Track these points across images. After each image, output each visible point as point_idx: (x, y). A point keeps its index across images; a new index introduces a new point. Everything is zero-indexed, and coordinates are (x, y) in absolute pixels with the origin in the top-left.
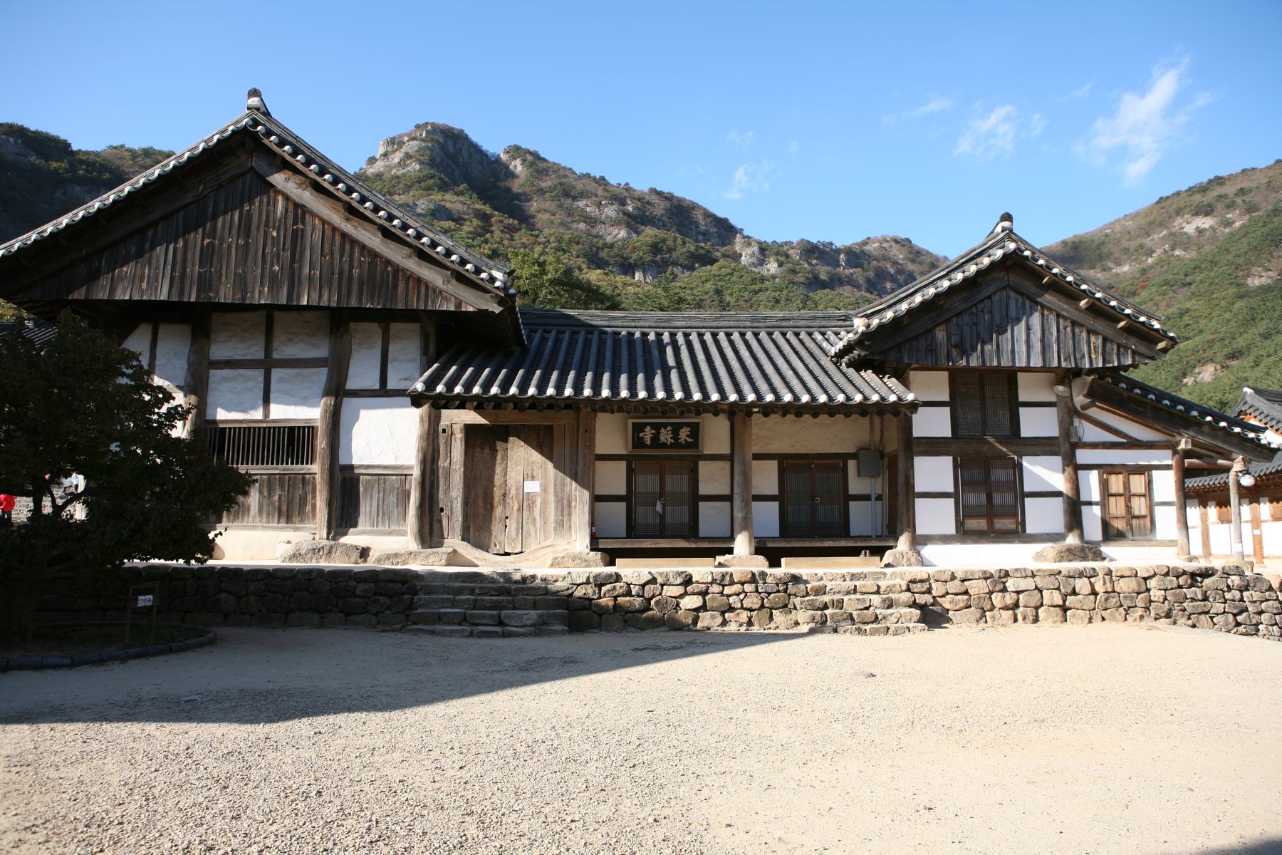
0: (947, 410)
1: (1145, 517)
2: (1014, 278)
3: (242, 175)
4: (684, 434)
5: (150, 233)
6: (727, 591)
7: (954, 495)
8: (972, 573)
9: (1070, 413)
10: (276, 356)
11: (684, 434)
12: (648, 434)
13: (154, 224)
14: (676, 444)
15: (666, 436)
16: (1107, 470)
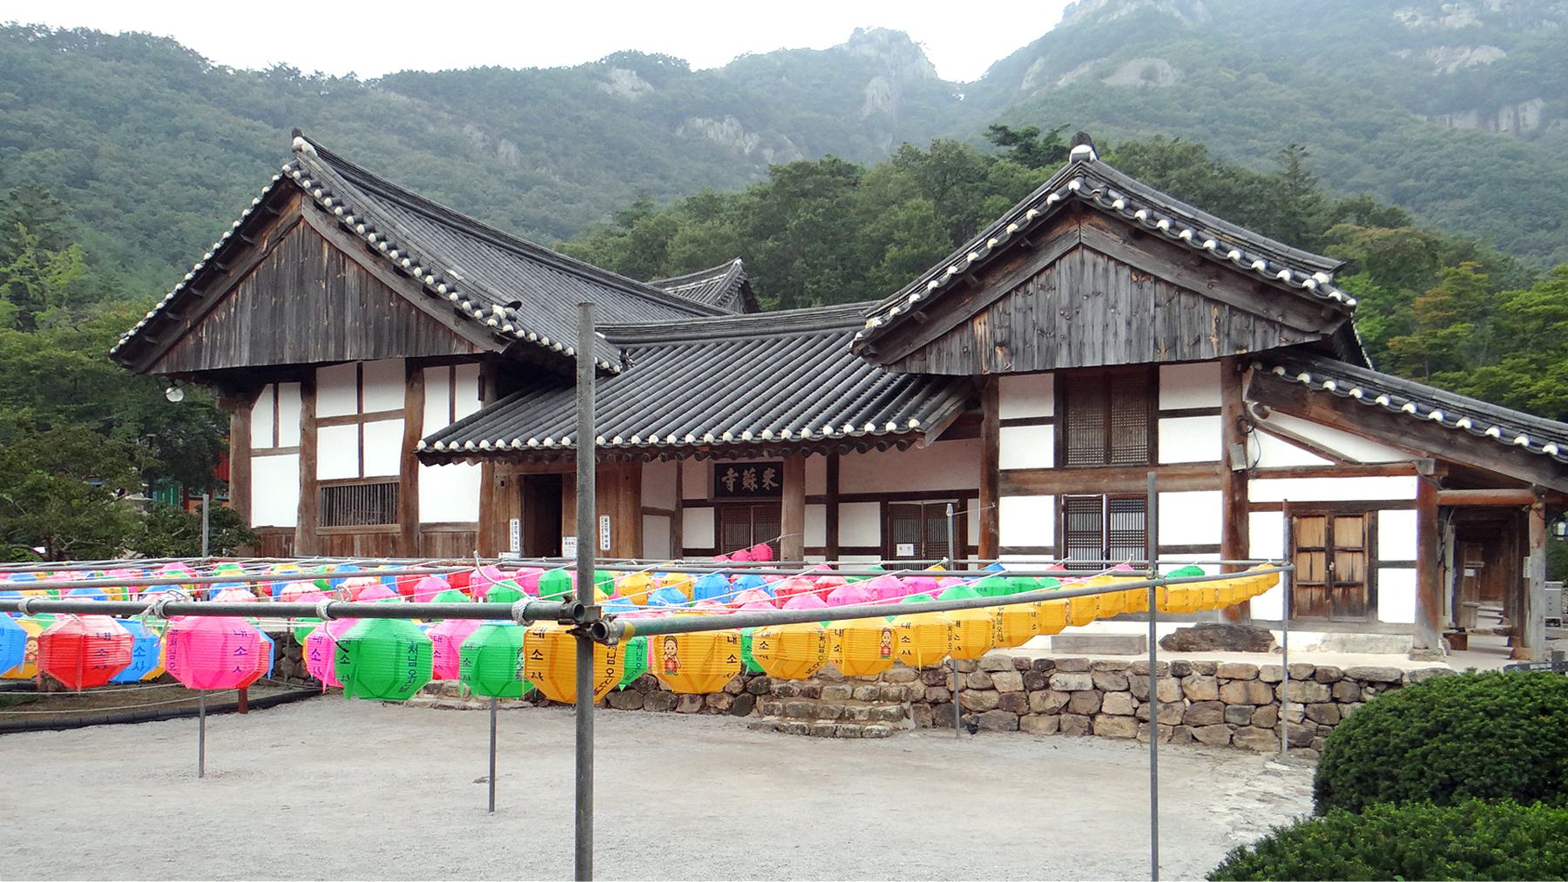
0: (1049, 430)
1: (1359, 585)
3: (296, 224)
7: (361, 478)
9: (1239, 430)
10: (365, 411)
12: (730, 478)
13: (234, 288)
15: (749, 482)
16: (1298, 511)
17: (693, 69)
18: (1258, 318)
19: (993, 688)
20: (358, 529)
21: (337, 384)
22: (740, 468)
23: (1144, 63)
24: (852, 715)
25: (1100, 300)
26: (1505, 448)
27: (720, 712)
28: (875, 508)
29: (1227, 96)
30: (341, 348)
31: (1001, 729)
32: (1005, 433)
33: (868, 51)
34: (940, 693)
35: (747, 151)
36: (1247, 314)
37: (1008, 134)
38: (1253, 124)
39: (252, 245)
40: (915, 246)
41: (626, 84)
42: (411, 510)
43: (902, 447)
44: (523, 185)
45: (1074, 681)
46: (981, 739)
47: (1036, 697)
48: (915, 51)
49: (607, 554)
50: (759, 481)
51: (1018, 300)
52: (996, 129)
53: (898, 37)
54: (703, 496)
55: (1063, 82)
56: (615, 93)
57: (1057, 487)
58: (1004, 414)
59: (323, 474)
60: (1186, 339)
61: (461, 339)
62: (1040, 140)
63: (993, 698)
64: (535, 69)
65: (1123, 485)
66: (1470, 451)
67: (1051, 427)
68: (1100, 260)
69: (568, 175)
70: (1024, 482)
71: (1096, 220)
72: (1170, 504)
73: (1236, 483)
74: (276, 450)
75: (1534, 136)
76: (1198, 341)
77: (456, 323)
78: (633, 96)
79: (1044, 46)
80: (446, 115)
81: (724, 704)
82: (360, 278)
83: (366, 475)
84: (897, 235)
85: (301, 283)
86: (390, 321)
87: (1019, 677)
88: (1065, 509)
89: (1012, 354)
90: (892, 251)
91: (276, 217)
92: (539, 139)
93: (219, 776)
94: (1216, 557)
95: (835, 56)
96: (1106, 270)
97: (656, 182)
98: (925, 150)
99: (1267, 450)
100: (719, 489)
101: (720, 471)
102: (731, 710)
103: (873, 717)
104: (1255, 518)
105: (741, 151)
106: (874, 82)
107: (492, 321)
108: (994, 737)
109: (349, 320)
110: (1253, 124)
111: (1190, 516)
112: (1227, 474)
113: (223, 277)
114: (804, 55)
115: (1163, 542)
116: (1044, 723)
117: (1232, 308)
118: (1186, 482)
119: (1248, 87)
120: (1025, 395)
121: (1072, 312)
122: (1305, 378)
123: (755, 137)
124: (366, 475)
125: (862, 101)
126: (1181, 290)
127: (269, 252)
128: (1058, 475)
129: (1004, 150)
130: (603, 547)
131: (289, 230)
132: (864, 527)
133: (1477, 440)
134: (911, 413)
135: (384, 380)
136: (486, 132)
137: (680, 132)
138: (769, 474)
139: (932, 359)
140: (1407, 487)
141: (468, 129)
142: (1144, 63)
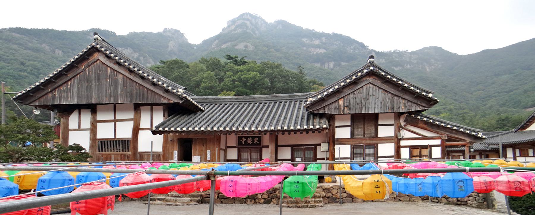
0: (349, 129)
2: (371, 79)
3: (96, 62)
4: (256, 140)
5: (69, 83)
9: (399, 128)
10: (117, 118)
11: (256, 140)
12: (243, 141)
13: (70, 80)
14: (253, 144)
16: (412, 148)
18: (415, 103)
19: (345, 192)
20: (113, 154)
21: (107, 110)
22: (247, 138)
23: (245, 44)
24: (309, 202)
25: (374, 97)
26: (463, 133)
27: (261, 203)
29: (265, 54)
30: (110, 100)
31: (348, 202)
33: (169, 34)
34: (330, 195)
36: (411, 102)
39: (77, 67)
42: (136, 147)
43: (320, 132)
48: (182, 35)
49: (209, 161)
50: (253, 141)
51: (352, 96)
53: (177, 32)
54: (235, 145)
55: (224, 46)
57: (351, 143)
58: (336, 125)
60: (396, 107)
61: (164, 98)
62: (239, 59)
63: (345, 195)
65: (368, 142)
66: (456, 134)
67: (350, 128)
68: (374, 87)
70: (342, 142)
71: (374, 77)
73: (397, 141)
74: (79, 129)
75: (332, 70)
76: (399, 108)
77: (163, 93)
79: (218, 37)
81: (262, 201)
82: (124, 79)
83: (117, 137)
84: (204, 80)
85: (98, 79)
86: (137, 92)
88: (353, 148)
89: (350, 109)
90: (203, 85)
91: (88, 59)
94: (393, 158)
95: (159, 34)
96: (376, 89)
98: (208, 59)
99: (405, 134)
100: (240, 143)
101: (240, 138)
102: (264, 203)
103: (315, 202)
104: (402, 149)
106: (171, 42)
107: (180, 93)
108: (346, 204)
111: (386, 149)
112: (396, 139)
113: (65, 76)
114: (150, 34)
115: (379, 155)
117: (408, 101)
118: (385, 141)
120: (342, 120)
121: (367, 99)
122: (419, 117)
123: (137, 54)
124: (117, 137)
125: (168, 47)
126: (396, 95)
127: (84, 70)
128: (352, 140)
129: (229, 61)
130: (208, 159)
131: (93, 63)
132: (286, 153)
133: (457, 132)
134: (184, 126)
135: (125, 109)
136: (51, 47)
139: (326, 109)
140: (438, 142)
142: (245, 44)
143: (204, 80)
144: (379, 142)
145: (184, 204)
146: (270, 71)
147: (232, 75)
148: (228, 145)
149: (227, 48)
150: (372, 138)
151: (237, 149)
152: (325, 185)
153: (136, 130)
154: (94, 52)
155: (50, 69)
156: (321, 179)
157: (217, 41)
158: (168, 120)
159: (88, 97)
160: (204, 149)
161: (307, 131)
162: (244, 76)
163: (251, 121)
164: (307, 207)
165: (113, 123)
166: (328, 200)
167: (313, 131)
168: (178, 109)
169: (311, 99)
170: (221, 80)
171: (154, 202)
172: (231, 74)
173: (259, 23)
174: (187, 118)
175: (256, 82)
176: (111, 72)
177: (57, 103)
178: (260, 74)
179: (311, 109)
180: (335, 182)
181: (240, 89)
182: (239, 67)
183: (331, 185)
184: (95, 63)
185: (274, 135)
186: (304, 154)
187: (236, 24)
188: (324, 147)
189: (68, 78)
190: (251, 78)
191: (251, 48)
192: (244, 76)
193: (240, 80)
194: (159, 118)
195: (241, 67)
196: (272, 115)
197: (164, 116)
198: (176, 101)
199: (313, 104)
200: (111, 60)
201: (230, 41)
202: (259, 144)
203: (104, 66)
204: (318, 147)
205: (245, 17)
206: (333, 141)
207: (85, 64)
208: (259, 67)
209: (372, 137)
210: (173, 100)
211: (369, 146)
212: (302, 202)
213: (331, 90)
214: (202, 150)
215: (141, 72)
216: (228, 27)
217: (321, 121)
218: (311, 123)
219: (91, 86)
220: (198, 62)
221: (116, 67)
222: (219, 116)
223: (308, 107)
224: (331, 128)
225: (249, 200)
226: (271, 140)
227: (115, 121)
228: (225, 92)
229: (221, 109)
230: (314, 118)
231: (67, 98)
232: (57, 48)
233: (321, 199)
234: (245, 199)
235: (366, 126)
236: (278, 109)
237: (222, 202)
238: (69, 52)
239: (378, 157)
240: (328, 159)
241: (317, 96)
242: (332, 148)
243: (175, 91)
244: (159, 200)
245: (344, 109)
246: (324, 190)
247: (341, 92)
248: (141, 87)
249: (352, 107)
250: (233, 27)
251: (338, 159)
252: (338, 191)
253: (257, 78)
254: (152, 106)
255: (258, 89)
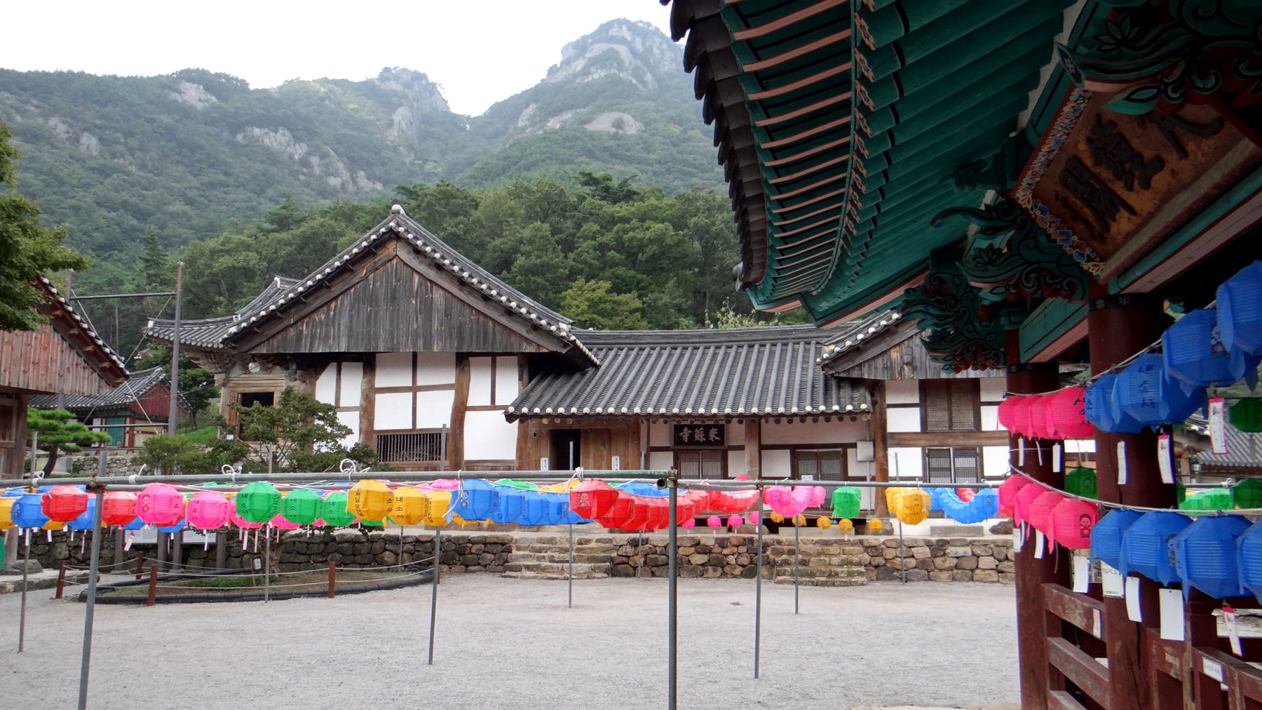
0: (917, 410)
5: (333, 306)
6: (725, 552)
8: (916, 541)
10: (420, 383)
12: (686, 434)
13: (335, 298)
15: (699, 436)
17: (252, 87)
24: (837, 574)
27: (735, 576)
28: (788, 452)
29: (675, 145)
31: (919, 580)
32: (890, 412)
33: (394, 86)
34: (880, 560)
35: (296, 157)
37: (592, 179)
38: (695, 167)
40: (538, 257)
41: (193, 95)
42: (458, 450)
44: (104, 172)
45: (961, 551)
46: (908, 586)
47: (938, 561)
48: (432, 89)
50: (707, 436)
52: (583, 174)
53: (419, 77)
54: (668, 445)
55: (554, 123)
56: (184, 102)
57: (923, 442)
58: (889, 401)
59: (378, 426)
62: (615, 183)
63: (912, 562)
64: (114, 77)
65: (961, 442)
69: (142, 166)
70: (904, 440)
72: (989, 452)
78: (200, 106)
79: (535, 94)
80: (32, 108)
81: (738, 571)
83: (419, 426)
85: (393, 298)
86: (471, 329)
87: (928, 550)
88: (928, 455)
89: (914, 369)
90: (521, 261)
91: (375, 254)
92: (119, 135)
93: (576, 607)
97: (221, 177)
100: (678, 440)
101: (678, 429)
102: (743, 575)
103: (850, 574)
105: (291, 157)
106: (400, 111)
107: (563, 334)
108: (915, 584)
109: (436, 325)
110: (695, 167)
116: (944, 575)
119: (689, 139)
124: (419, 426)
127: (366, 278)
128: (923, 436)
129: (587, 189)
131: (384, 264)
135: (436, 362)
136: (70, 126)
137: (239, 138)
138: (713, 432)
139: (865, 369)
141: (53, 121)
142: (615, 115)
143: (523, 248)
144: (984, 442)
145: (580, 576)
146: (701, 220)
147: (599, 232)
148: (652, 445)
149: (562, 129)
150: (967, 434)
151: (671, 454)
152: (870, 539)
153: (460, 410)
154: (390, 239)
155: (63, 193)
156: (859, 524)
157: (532, 109)
158: (532, 389)
159: (370, 338)
160: (605, 453)
161: (827, 416)
162: (631, 234)
163: (707, 393)
164: (833, 585)
165: (410, 395)
166: (876, 572)
167: (840, 415)
168: (551, 365)
169: (832, 347)
170: (568, 246)
171: (519, 574)
172: (596, 227)
173: (656, 51)
174: (568, 386)
175: (665, 250)
176: (420, 285)
177: (305, 349)
178: (677, 227)
179: (832, 368)
180: (890, 532)
181: (621, 271)
182: (616, 208)
183: (882, 538)
184: (389, 265)
185: (754, 423)
186: (819, 468)
187: (588, 55)
188: (865, 450)
189: (333, 295)
190: (651, 241)
191: (632, 127)
192: (631, 234)
193: (620, 245)
194: (509, 388)
195: (622, 209)
196: (748, 379)
197: (521, 379)
198: (554, 349)
199: (837, 359)
200: (421, 258)
201: (572, 107)
202: (721, 442)
203: (406, 271)
204: (850, 451)
205: (614, 32)
206: (883, 440)
207: (369, 264)
208: (671, 206)
209: (969, 431)
210: (548, 347)
211: (963, 452)
212: (823, 574)
213: (871, 330)
214: (601, 456)
215: (484, 286)
216: (567, 62)
217: (856, 395)
218: (834, 400)
219: (376, 313)
220: (504, 193)
221: (432, 274)
222: (626, 374)
223: (826, 365)
224: (878, 410)
225: (710, 568)
226: (749, 433)
227: (414, 389)
228: (581, 281)
229: (634, 361)
230: (839, 387)
231: (327, 337)
232: (84, 130)
233: (862, 569)
234: (703, 565)
235: (954, 407)
236: (758, 364)
237: (653, 574)
238: (116, 142)
239: (983, 477)
240: (873, 479)
241: (843, 341)
242: (880, 454)
243: (553, 328)
244: (528, 568)
245: (902, 369)
246: (867, 548)
247: (894, 333)
248: (481, 318)
249: (918, 364)
250: (579, 65)
251: (894, 479)
252: (898, 552)
253: (669, 241)
254: (494, 358)
255: (670, 271)
